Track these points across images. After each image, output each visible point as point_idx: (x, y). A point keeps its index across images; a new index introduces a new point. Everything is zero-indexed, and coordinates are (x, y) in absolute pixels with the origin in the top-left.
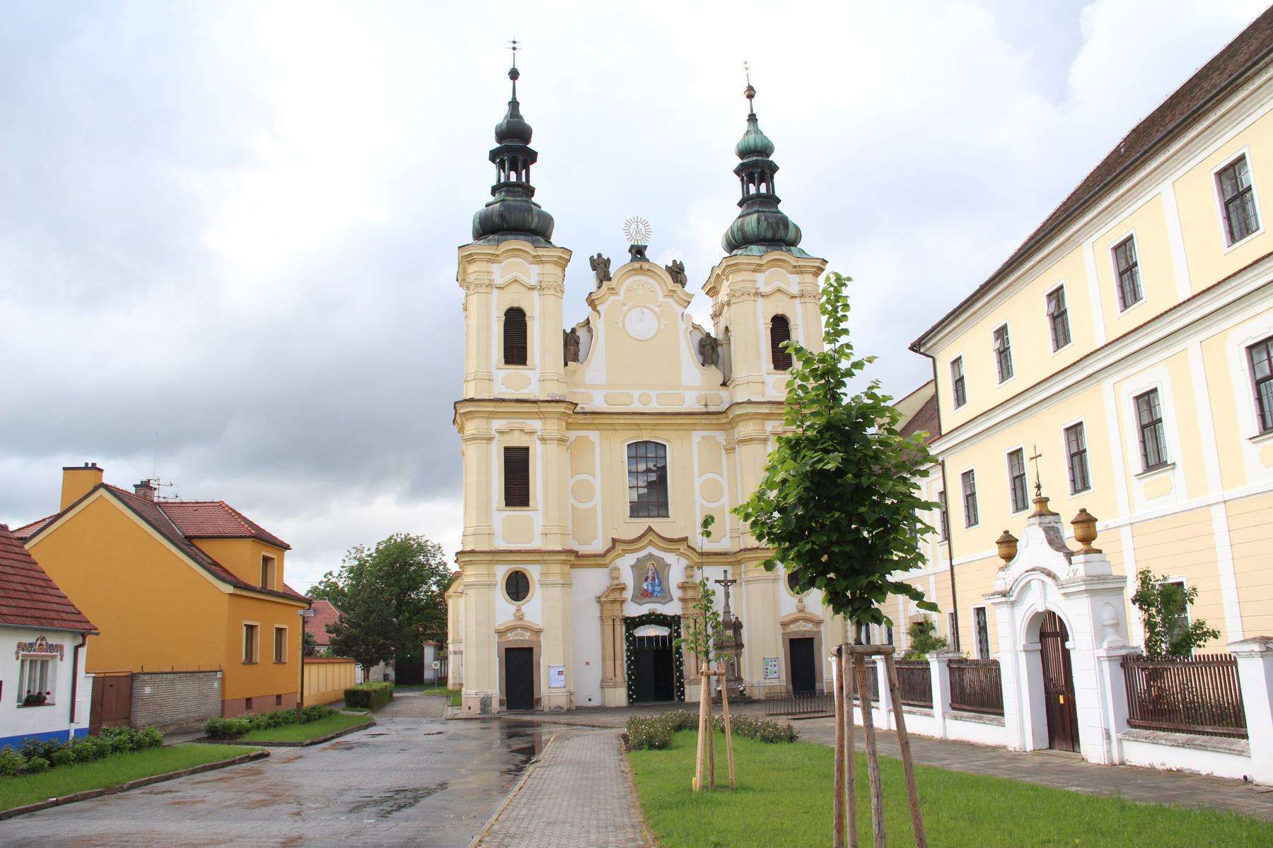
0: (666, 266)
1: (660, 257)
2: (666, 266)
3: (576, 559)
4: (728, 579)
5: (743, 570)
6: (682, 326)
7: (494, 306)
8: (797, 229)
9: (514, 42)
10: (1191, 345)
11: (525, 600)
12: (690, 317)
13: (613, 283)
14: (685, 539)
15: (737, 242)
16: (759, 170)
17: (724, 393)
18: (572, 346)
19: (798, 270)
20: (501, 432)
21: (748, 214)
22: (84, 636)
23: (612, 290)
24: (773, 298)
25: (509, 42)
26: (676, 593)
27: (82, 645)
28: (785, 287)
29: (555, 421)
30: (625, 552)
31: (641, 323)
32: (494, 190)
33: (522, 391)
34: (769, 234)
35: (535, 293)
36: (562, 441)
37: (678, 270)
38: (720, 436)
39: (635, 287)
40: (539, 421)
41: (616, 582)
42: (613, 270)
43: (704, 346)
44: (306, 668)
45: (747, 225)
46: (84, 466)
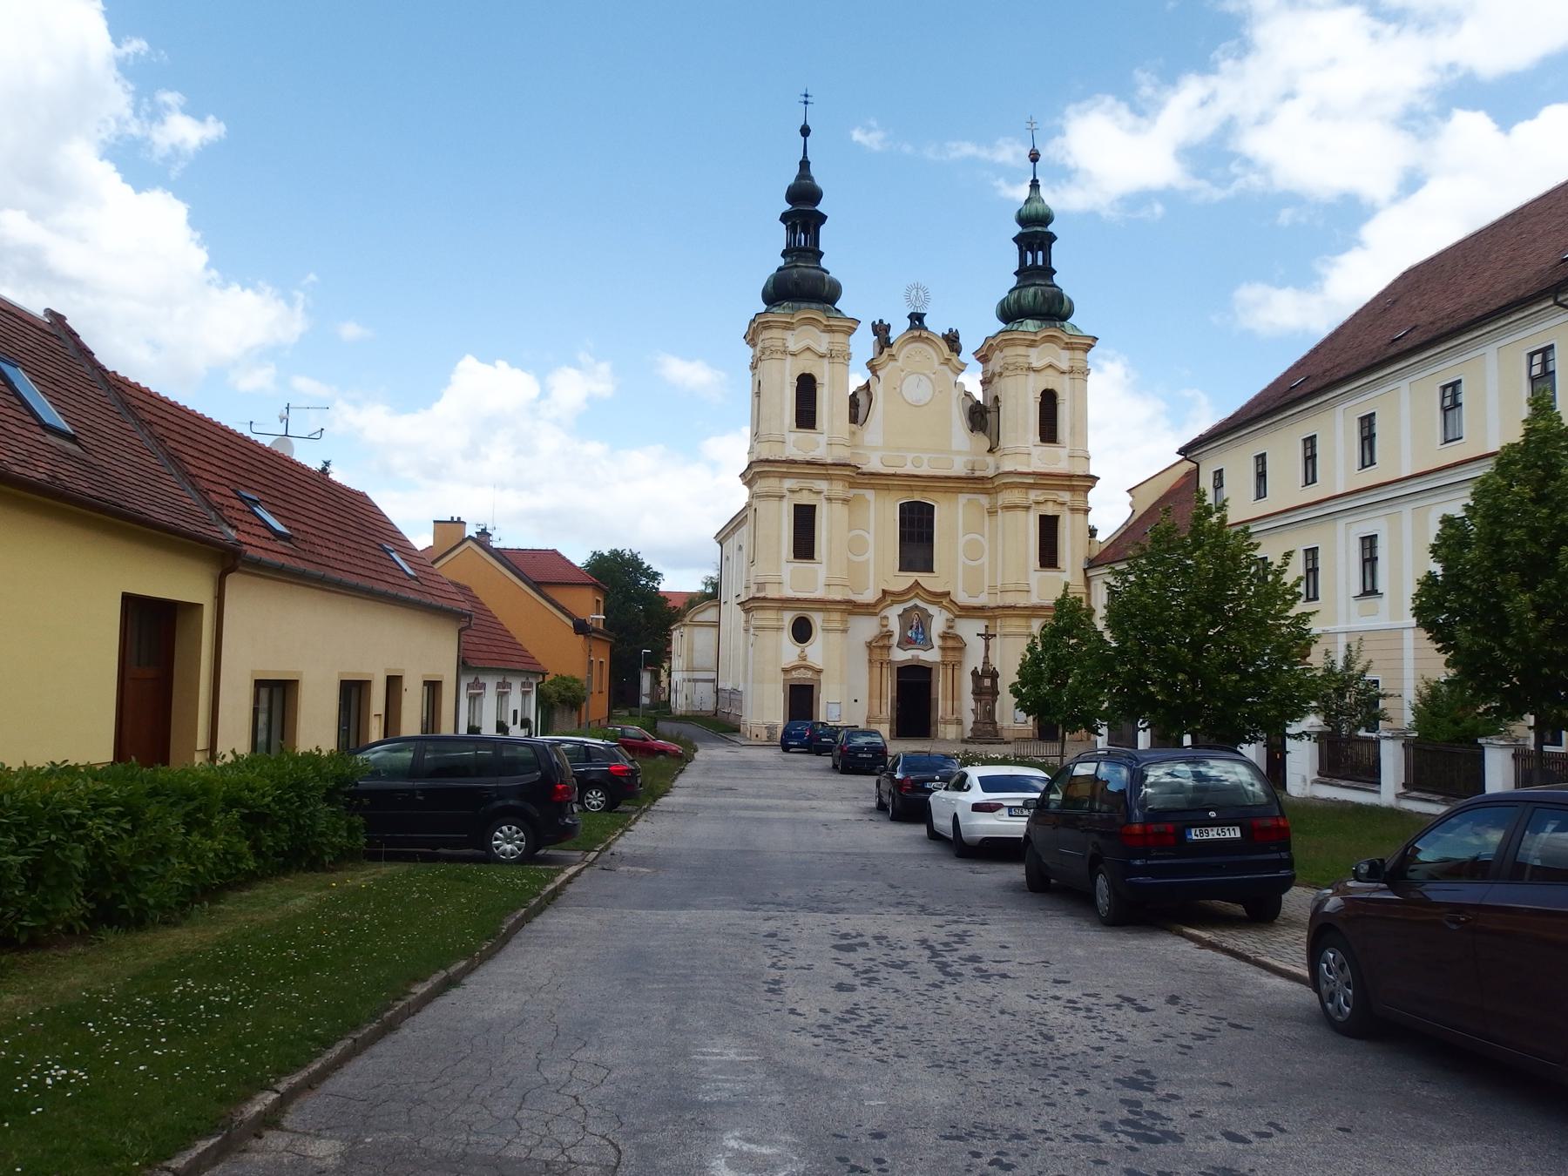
0: (943, 334)
1: (937, 324)
2: (943, 334)
3: (853, 608)
4: (989, 633)
5: (998, 624)
6: (955, 393)
7: (787, 372)
8: (1071, 303)
10: (1407, 511)
11: (798, 644)
12: (962, 385)
13: (894, 350)
14: (948, 594)
15: (1010, 313)
16: (1038, 241)
17: (990, 459)
18: (857, 407)
19: (1070, 347)
20: (792, 491)
21: (1025, 286)
23: (892, 356)
24: (1044, 373)
25: (801, 95)
26: (937, 642)
28: (1056, 362)
29: (840, 482)
30: (893, 602)
31: (917, 389)
32: (784, 254)
33: (812, 453)
34: (1045, 309)
35: (826, 361)
36: (846, 501)
37: (954, 338)
38: (984, 500)
39: (913, 353)
40: (825, 482)
41: (885, 629)
42: (894, 335)
43: (974, 413)
45: (1024, 299)
46: (450, 520)
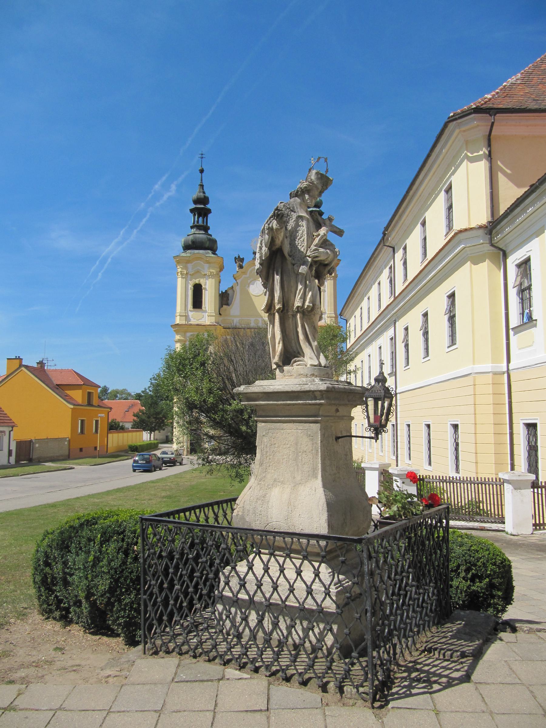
9: (202, 154)
22: (12, 427)
23: (244, 273)
27: (12, 430)
44: (110, 435)
